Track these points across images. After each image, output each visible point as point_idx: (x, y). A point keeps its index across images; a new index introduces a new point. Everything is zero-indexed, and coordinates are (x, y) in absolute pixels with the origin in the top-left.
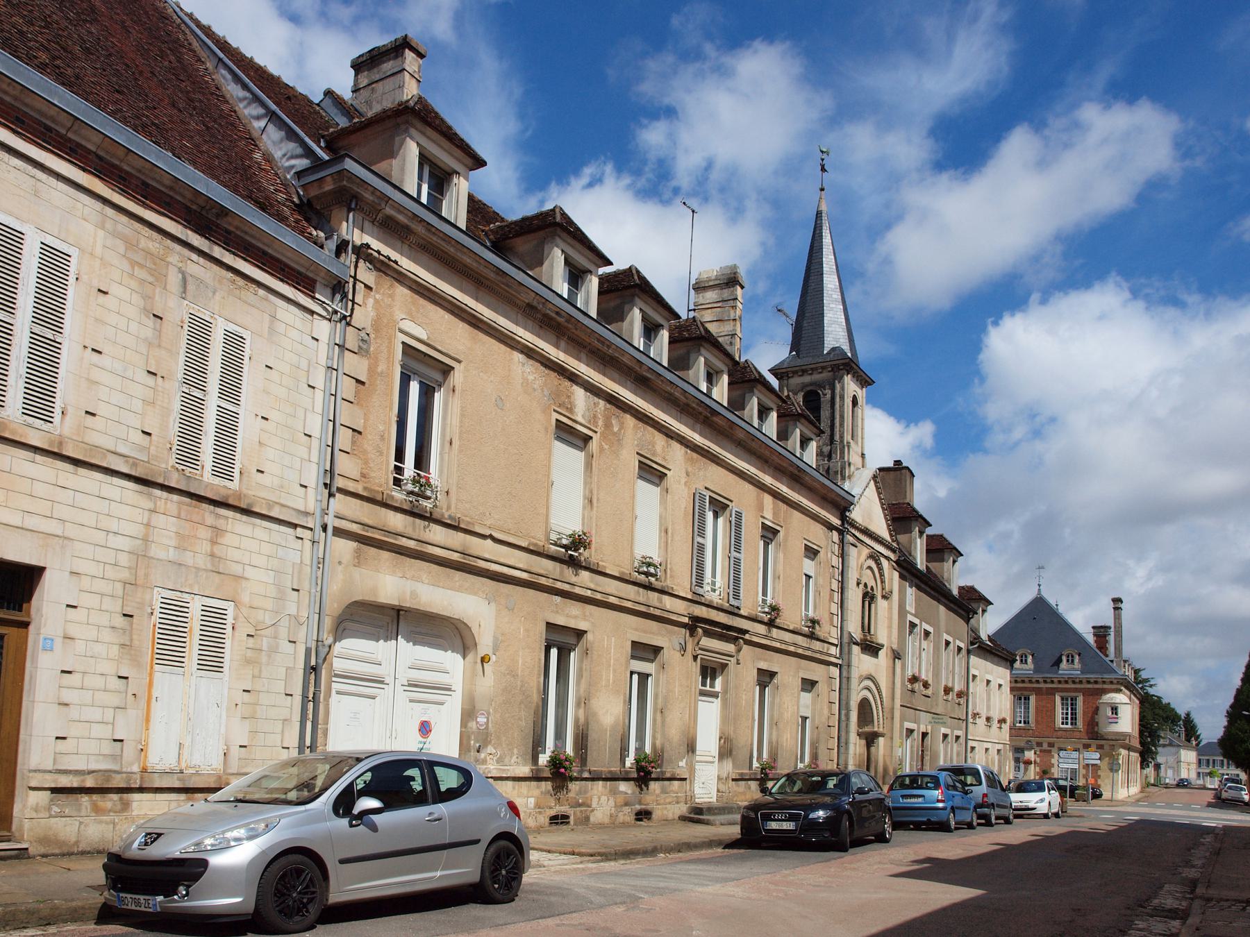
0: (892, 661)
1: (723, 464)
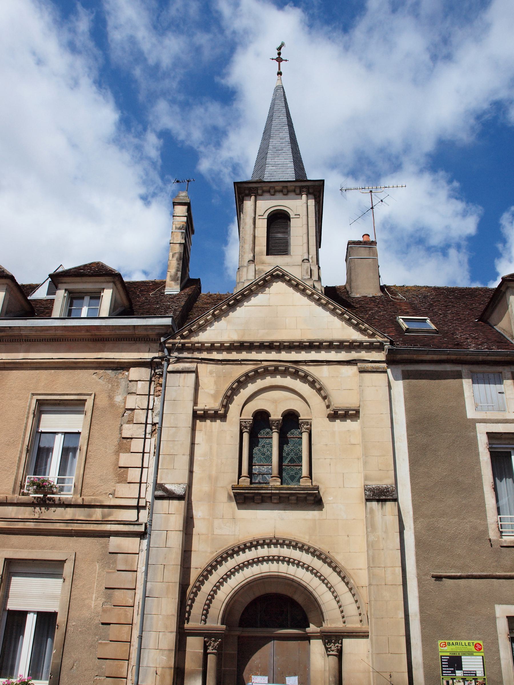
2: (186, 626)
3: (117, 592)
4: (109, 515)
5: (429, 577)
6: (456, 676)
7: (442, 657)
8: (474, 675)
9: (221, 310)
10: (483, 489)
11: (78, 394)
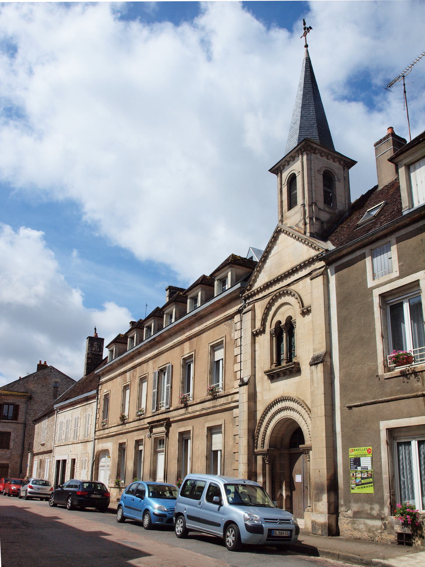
1: (165, 351)
2: (255, 450)
5: (345, 408)
6: (357, 470)
7: (351, 459)
8: (367, 469)
9: (260, 267)
10: (376, 339)
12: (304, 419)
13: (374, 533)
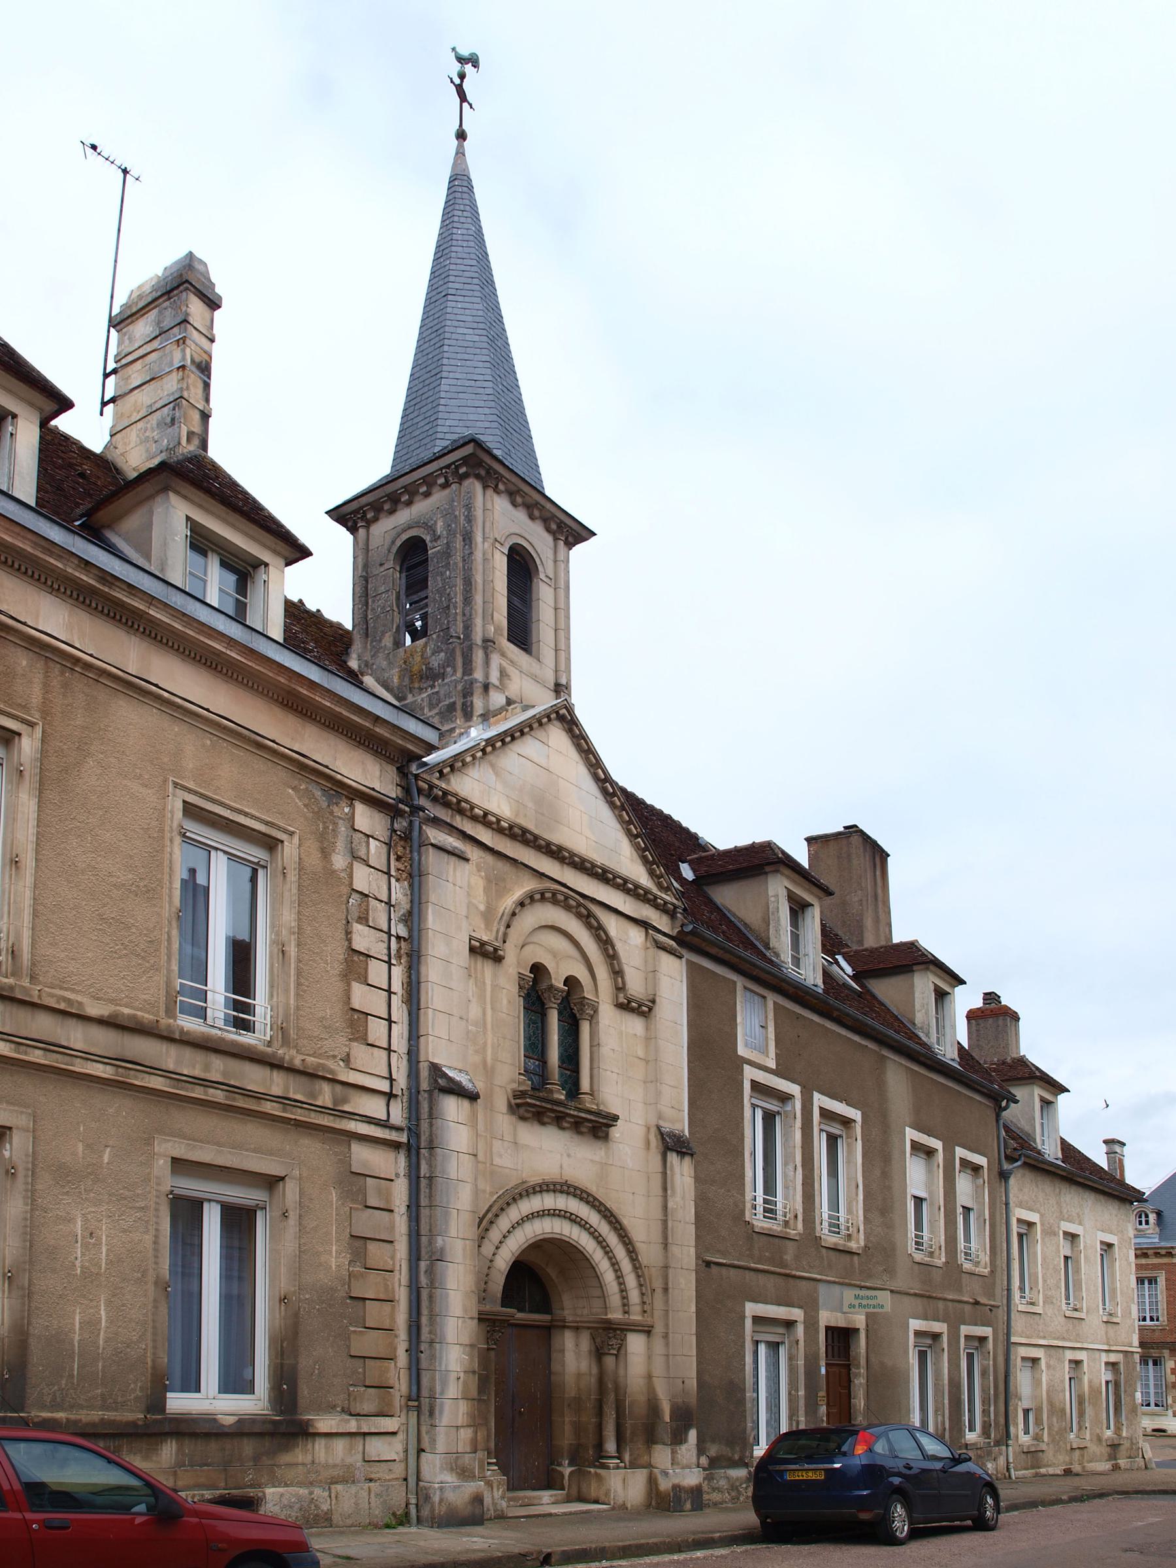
0: (659, 1158)
3: (372, 1247)
4: (345, 1100)
11: (202, 796)
12: (505, 1237)
13: (738, 1491)
